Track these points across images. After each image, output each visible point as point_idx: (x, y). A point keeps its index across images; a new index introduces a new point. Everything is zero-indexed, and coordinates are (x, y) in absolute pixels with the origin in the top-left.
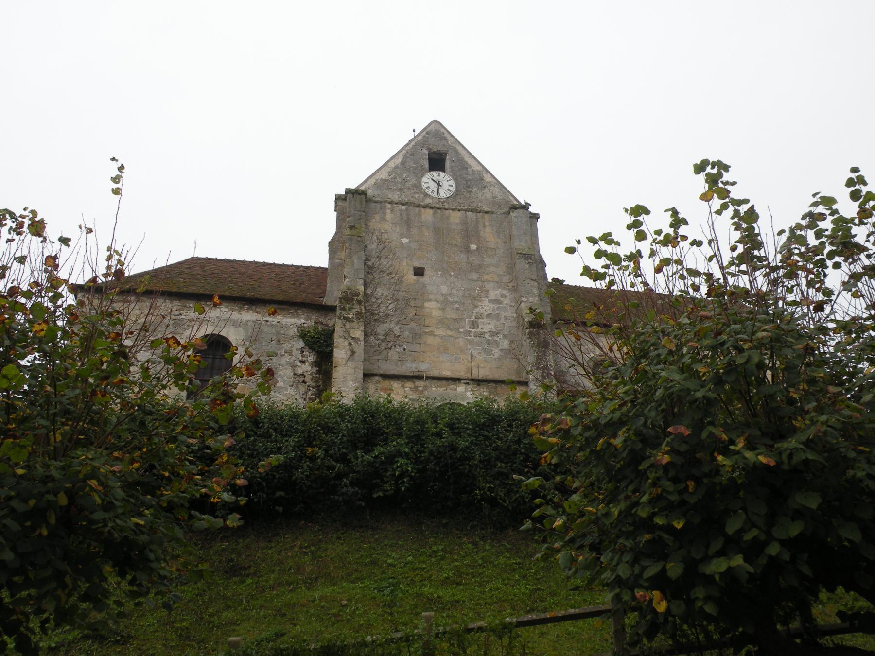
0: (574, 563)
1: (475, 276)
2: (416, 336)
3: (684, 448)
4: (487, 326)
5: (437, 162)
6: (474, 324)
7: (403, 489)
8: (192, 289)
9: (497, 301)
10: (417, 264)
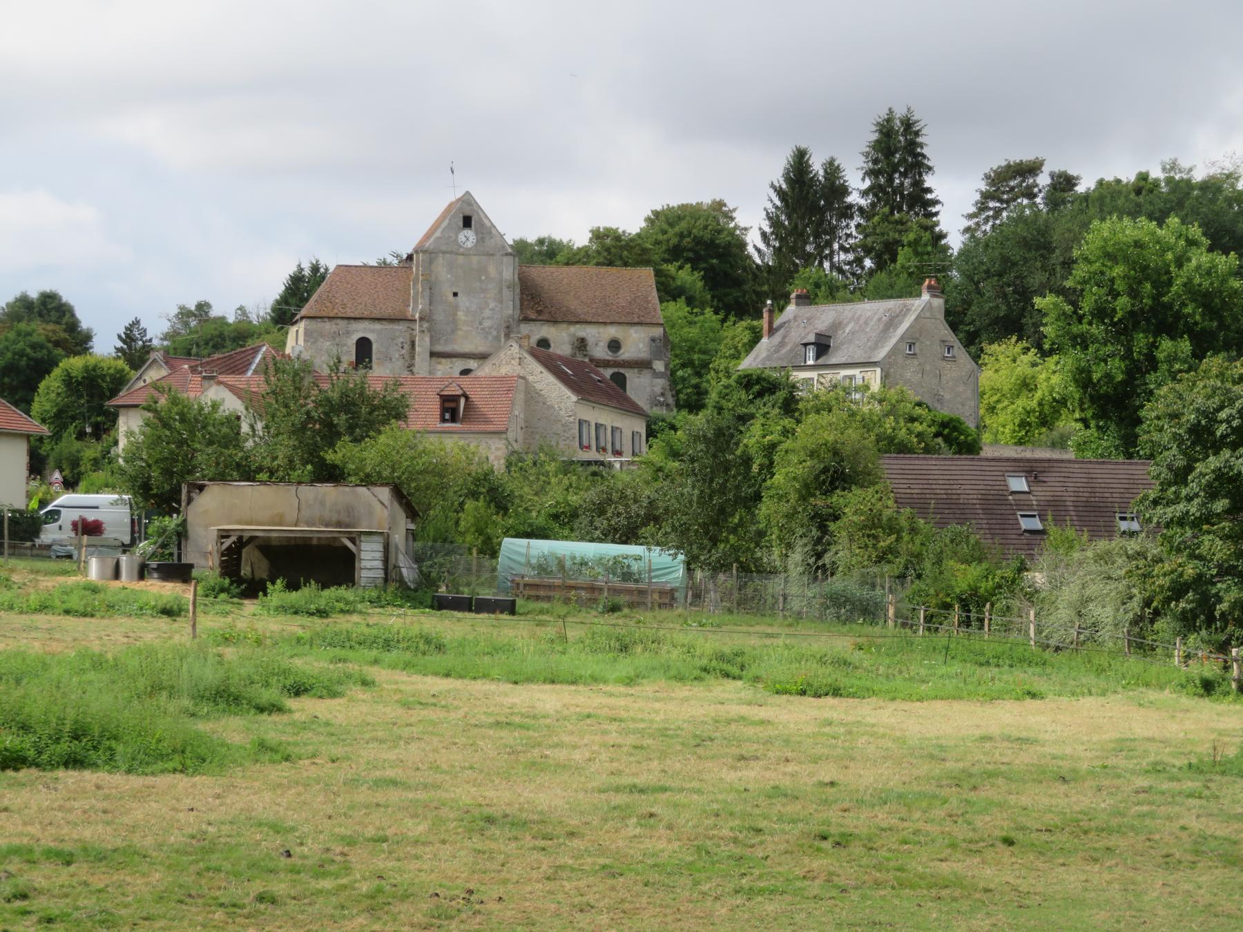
0: (1025, 392)
1: (482, 295)
2: (454, 331)
3: (372, 433)
4: (487, 323)
5: (467, 222)
6: (481, 323)
7: (769, 302)
8: (352, 315)
9: (492, 310)
10: (455, 290)
